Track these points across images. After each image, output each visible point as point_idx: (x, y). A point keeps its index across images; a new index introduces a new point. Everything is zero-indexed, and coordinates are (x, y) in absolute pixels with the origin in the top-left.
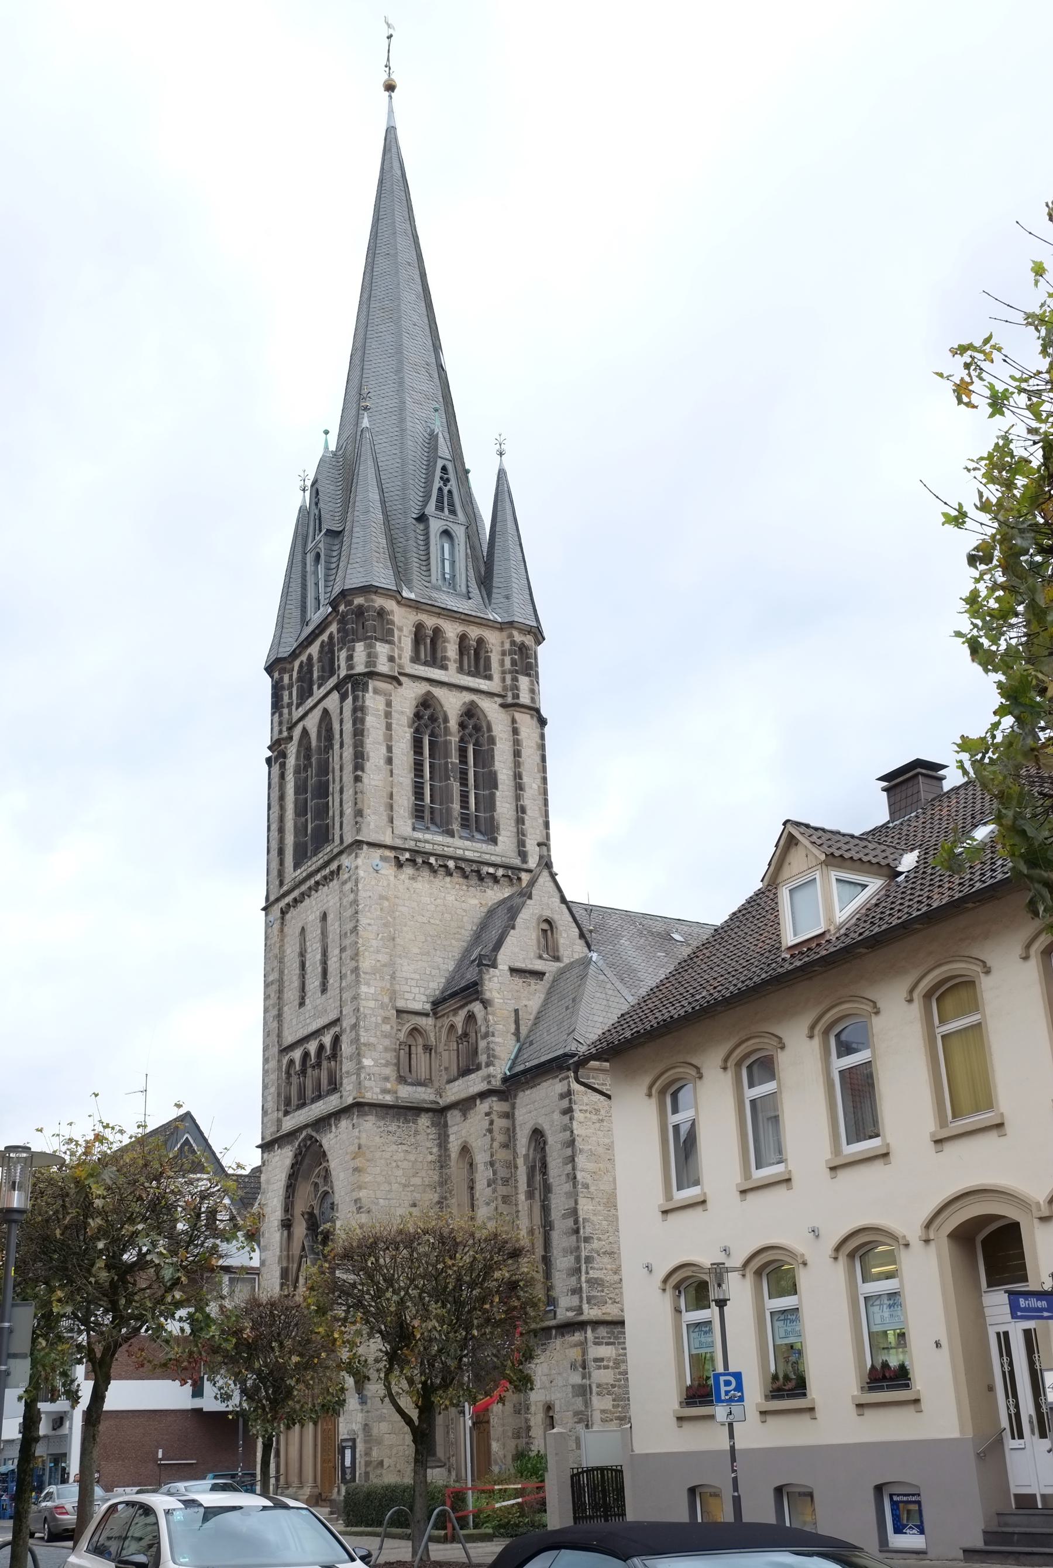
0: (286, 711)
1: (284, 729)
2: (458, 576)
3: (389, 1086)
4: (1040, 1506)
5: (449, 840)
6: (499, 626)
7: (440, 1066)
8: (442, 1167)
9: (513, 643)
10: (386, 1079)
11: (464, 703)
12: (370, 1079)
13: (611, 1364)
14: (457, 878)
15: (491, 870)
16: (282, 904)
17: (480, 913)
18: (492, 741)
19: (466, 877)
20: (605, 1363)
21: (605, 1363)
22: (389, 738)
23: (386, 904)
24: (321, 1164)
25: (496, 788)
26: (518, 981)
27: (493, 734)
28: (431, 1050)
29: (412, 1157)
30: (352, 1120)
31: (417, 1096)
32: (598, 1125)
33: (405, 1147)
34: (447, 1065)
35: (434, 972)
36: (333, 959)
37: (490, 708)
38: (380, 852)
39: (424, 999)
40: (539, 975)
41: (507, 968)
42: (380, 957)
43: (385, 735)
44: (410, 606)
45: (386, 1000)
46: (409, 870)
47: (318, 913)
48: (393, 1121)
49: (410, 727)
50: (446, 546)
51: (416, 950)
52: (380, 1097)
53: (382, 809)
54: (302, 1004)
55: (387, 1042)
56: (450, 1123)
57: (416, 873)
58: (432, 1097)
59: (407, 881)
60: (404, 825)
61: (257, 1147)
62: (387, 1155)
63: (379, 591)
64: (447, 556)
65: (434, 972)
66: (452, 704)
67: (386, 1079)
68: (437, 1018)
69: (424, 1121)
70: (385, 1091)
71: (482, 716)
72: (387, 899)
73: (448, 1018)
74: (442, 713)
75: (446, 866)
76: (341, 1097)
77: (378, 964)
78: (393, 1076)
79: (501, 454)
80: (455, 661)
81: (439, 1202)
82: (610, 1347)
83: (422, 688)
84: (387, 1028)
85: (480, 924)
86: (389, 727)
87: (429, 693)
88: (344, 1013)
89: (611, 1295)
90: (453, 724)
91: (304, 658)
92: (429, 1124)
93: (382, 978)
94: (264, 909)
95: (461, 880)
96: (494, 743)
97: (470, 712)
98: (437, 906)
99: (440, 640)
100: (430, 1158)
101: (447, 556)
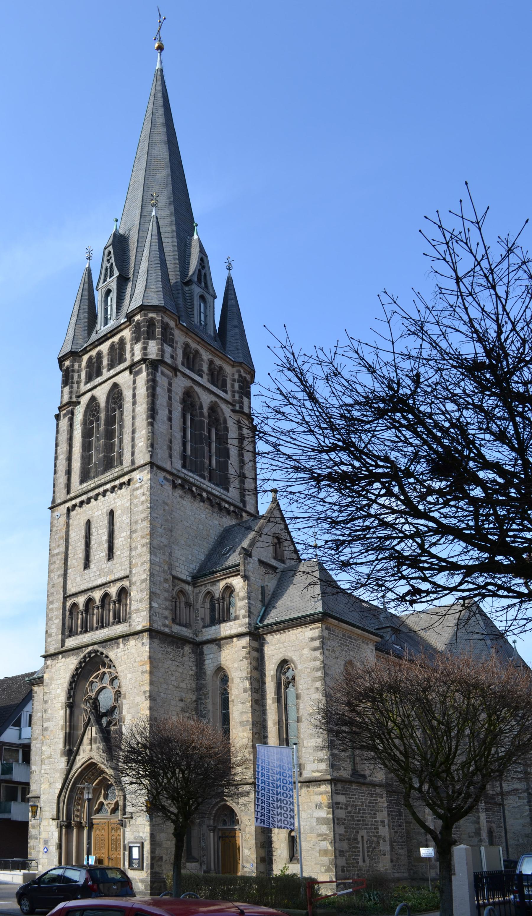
0: (75, 385)
1: (74, 396)
2: (209, 325)
3: (167, 622)
4: (74, 864)
5: (202, 480)
6: (232, 363)
7: (196, 617)
8: (197, 679)
9: (240, 376)
10: (166, 618)
11: (212, 402)
12: (156, 616)
13: (344, 806)
14: (207, 505)
15: (227, 506)
16: (69, 504)
17: (218, 530)
18: (226, 429)
19: (212, 506)
20: (341, 806)
21: (341, 806)
22: (170, 405)
23: (167, 508)
24: (99, 669)
25: (229, 458)
26: (263, 570)
27: (228, 426)
28: (190, 606)
29: (181, 670)
30: (142, 640)
31: (182, 633)
32: (335, 660)
33: (176, 663)
34: (203, 617)
35: (193, 559)
36: (120, 539)
37: (226, 410)
38: (164, 474)
39: (187, 573)
40: (274, 569)
41: (257, 559)
42: (163, 540)
43: (168, 403)
44: (182, 331)
45: (166, 568)
46: (179, 492)
47: (105, 510)
48: (169, 645)
49: (181, 404)
50: (202, 305)
51: (183, 543)
52: (162, 628)
53: (165, 448)
54: (87, 566)
55: (166, 595)
56: (205, 652)
57: (184, 495)
58: (191, 635)
59: (178, 498)
60: (178, 464)
61: (41, 656)
62: (167, 666)
63: (167, 312)
64: (202, 310)
65: (193, 559)
66: (206, 399)
67: (166, 618)
68: (194, 587)
69: (188, 649)
70: (165, 625)
71: (220, 413)
72: (168, 505)
73: (206, 587)
74: (199, 403)
75: (201, 495)
76: (130, 626)
77: (162, 544)
78: (170, 618)
79: (229, 269)
80: (207, 374)
81: (196, 701)
82: (343, 796)
83: (189, 383)
84: (166, 586)
85: (220, 536)
86: (170, 398)
87: (192, 387)
88: (134, 572)
89: (343, 765)
90: (205, 411)
91: (94, 353)
92: (190, 651)
93: (164, 554)
94: (50, 508)
95: (209, 507)
96: (228, 431)
97: (213, 408)
98: (195, 518)
99: (198, 360)
100: (191, 673)
101: (202, 310)
